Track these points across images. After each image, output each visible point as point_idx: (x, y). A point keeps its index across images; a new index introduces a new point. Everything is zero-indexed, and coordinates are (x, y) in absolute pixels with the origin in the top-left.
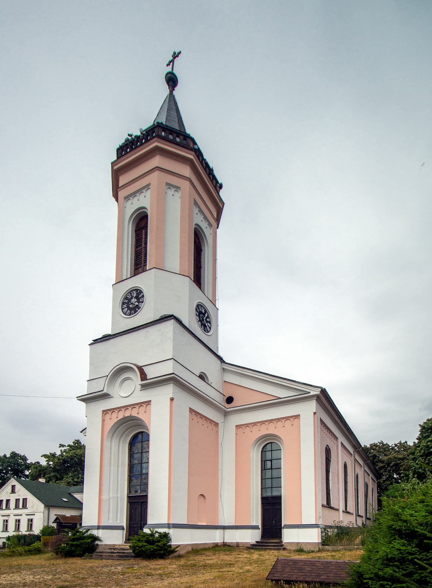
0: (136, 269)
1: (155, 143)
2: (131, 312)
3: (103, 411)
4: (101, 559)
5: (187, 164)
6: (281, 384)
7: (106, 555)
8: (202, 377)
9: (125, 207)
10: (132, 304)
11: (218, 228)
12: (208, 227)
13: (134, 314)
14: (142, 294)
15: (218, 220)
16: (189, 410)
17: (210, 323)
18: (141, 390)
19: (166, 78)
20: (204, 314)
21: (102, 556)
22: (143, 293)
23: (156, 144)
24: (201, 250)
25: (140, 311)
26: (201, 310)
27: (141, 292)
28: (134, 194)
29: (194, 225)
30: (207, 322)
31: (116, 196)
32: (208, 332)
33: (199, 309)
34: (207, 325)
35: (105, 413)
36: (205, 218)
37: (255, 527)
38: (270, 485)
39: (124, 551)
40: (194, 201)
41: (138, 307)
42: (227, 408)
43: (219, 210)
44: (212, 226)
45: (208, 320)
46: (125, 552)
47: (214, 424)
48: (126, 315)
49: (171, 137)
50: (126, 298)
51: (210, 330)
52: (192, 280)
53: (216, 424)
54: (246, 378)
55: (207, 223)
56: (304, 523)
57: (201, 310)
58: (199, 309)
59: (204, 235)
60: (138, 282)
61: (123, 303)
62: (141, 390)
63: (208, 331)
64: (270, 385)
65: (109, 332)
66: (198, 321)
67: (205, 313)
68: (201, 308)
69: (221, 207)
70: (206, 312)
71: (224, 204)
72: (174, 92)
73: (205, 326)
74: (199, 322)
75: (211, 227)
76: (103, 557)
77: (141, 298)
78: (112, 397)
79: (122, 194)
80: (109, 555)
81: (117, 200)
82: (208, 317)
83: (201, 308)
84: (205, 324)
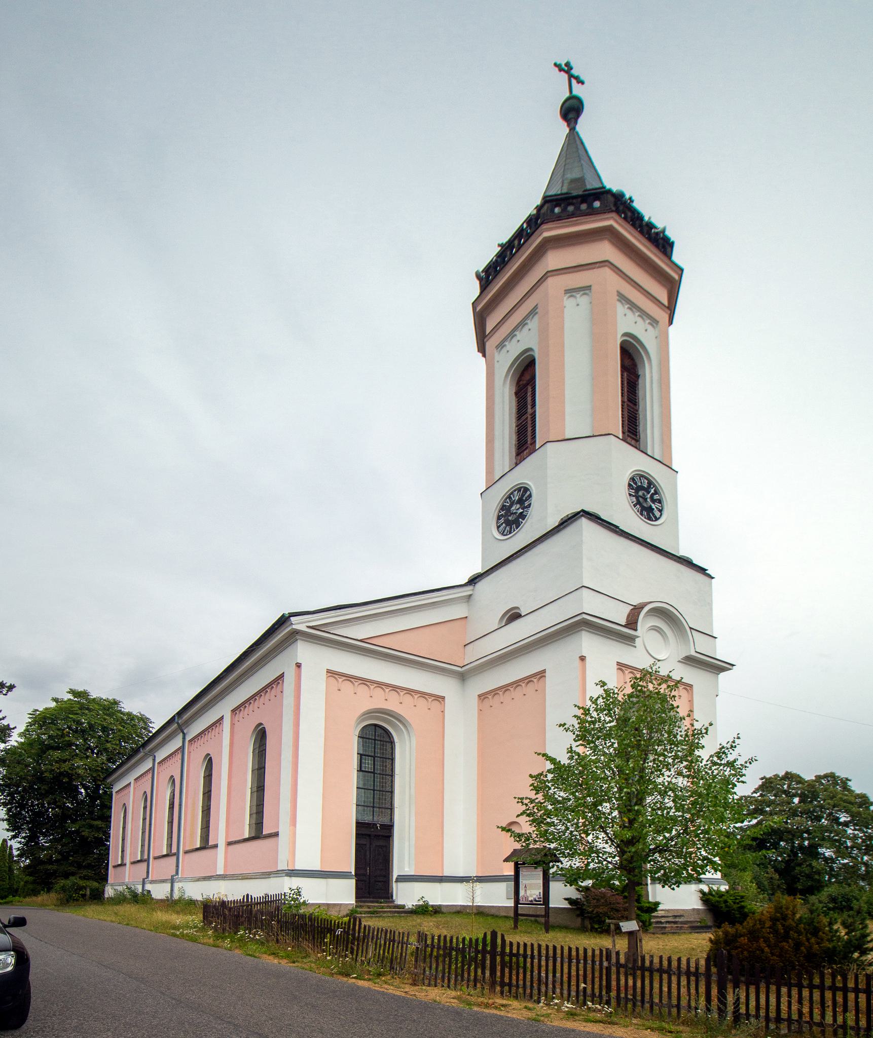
0: (518, 454)
1: (549, 232)
2: (511, 528)
3: (479, 696)
4: (662, 933)
5: (664, 286)
6: (366, 616)
7: (672, 927)
8: (513, 616)
9: (656, 338)
10: (512, 513)
11: (671, 322)
12: (650, 328)
13: (517, 528)
14: (528, 493)
15: (671, 308)
16: (616, 667)
17: (660, 501)
18: (679, 661)
19: (563, 108)
20: (647, 490)
21: (665, 928)
22: (529, 490)
23: (610, 222)
24: (638, 377)
25: (526, 522)
26: (641, 483)
27: (526, 490)
28: (511, 335)
29: (619, 335)
30: (653, 501)
31: (482, 349)
32: (657, 519)
33: (636, 483)
34: (654, 507)
35: (482, 697)
36: (644, 314)
37: (403, 879)
38: (370, 801)
39: (677, 920)
40: (618, 295)
41: (522, 516)
42: (461, 667)
43: (673, 286)
44: (657, 322)
45: (656, 497)
46: (678, 922)
47: (683, 686)
48: (504, 535)
49: (571, 208)
50: (503, 508)
51: (661, 515)
52: (619, 438)
53: (440, 699)
54: (433, 608)
55: (648, 321)
56: (447, 873)
57: (641, 483)
58: (636, 483)
59: (639, 344)
60: (525, 474)
61: (499, 518)
62: (679, 661)
63: (655, 517)
64: (383, 619)
65: (479, 570)
66: (634, 505)
67: (649, 487)
68: (640, 480)
69: (673, 278)
70: (650, 483)
71: (473, 304)
72: (578, 128)
73: (650, 510)
74: (635, 507)
75: (657, 324)
76: (667, 929)
77: (526, 500)
78: (635, 647)
79: (490, 345)
80: (677, 927)
81: (484, 356)
82: (656, 492)
83: (640, 480)
84: (651, 506)
